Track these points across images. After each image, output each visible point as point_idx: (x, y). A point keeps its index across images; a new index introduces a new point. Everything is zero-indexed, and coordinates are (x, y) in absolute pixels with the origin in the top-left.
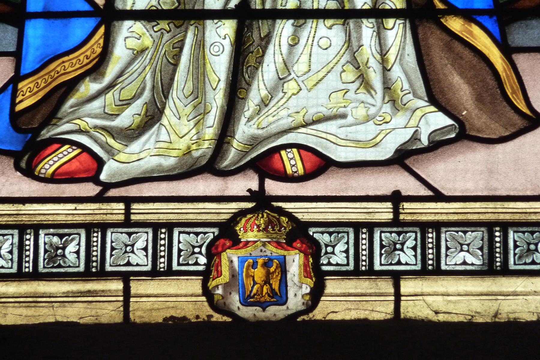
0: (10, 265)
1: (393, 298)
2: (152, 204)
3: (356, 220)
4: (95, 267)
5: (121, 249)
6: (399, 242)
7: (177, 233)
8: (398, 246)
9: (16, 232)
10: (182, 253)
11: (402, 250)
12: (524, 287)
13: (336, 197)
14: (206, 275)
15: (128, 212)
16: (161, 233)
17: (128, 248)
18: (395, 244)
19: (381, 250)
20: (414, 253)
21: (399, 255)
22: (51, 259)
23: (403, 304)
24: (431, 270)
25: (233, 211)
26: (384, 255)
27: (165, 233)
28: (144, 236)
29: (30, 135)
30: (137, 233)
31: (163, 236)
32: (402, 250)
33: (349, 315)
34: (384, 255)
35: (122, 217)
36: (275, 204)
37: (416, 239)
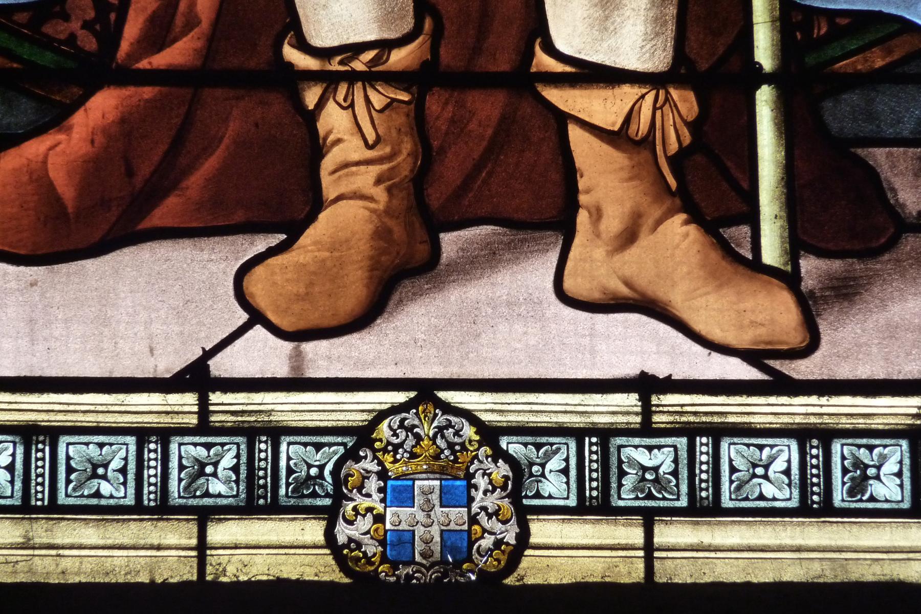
0: (122, 494)
1: (641, 553)
2: (147, 394)
3: (72, 424)
4: (40, 497)
5: (85, 470)
6: (761, 463)
7: (727, 445)
8: (209, 469)
9: (131, 440)
10: (73, 477)
11: (877, 478)
12: (792, 538)
13: (328, 380)
14: (331, 515)
15: (647, 411)
16: (812, 447)
17: (760, 471)
18: (203, 465)
19: (180, 472)
20: (565, 480)
21: (760, 484)
22: (858, 487)
23: (657, 564)
24: (705, 509)
25: (378, 407)
26: (74, 483)
27: (817, 447)
28: (627, 452)
29: (750, 257)
30: (111, 445)
31: (814, 452)
32: (877, 478)
33: (247, 574)
34: (74, 483)
35: (193, 420)
36: (412, 394)
37: (238, 456)
